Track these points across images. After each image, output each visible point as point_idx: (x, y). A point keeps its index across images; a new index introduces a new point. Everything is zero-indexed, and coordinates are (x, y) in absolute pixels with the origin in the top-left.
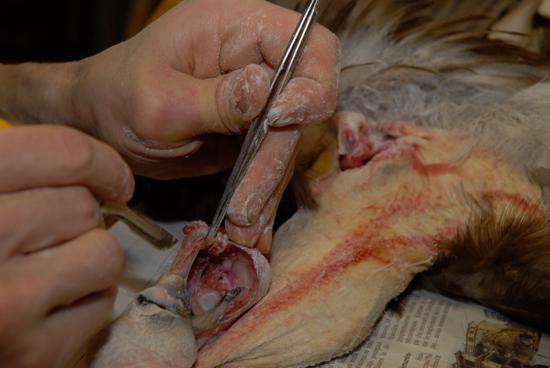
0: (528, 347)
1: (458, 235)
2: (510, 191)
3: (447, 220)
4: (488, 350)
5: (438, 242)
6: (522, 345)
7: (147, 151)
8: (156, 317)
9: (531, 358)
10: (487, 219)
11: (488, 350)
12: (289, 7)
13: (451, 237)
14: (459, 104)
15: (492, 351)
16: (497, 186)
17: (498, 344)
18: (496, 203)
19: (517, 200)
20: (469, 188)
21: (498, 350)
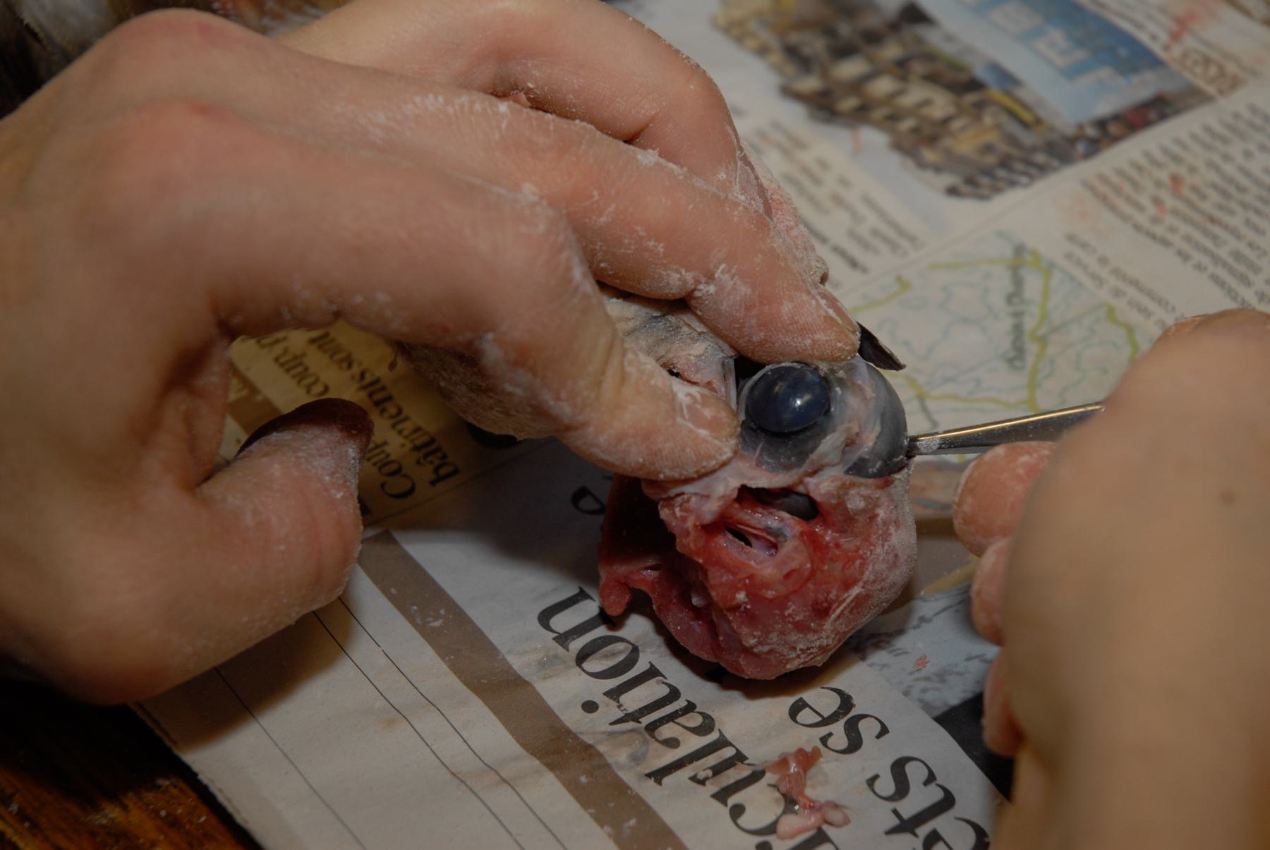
15: (816, 45)
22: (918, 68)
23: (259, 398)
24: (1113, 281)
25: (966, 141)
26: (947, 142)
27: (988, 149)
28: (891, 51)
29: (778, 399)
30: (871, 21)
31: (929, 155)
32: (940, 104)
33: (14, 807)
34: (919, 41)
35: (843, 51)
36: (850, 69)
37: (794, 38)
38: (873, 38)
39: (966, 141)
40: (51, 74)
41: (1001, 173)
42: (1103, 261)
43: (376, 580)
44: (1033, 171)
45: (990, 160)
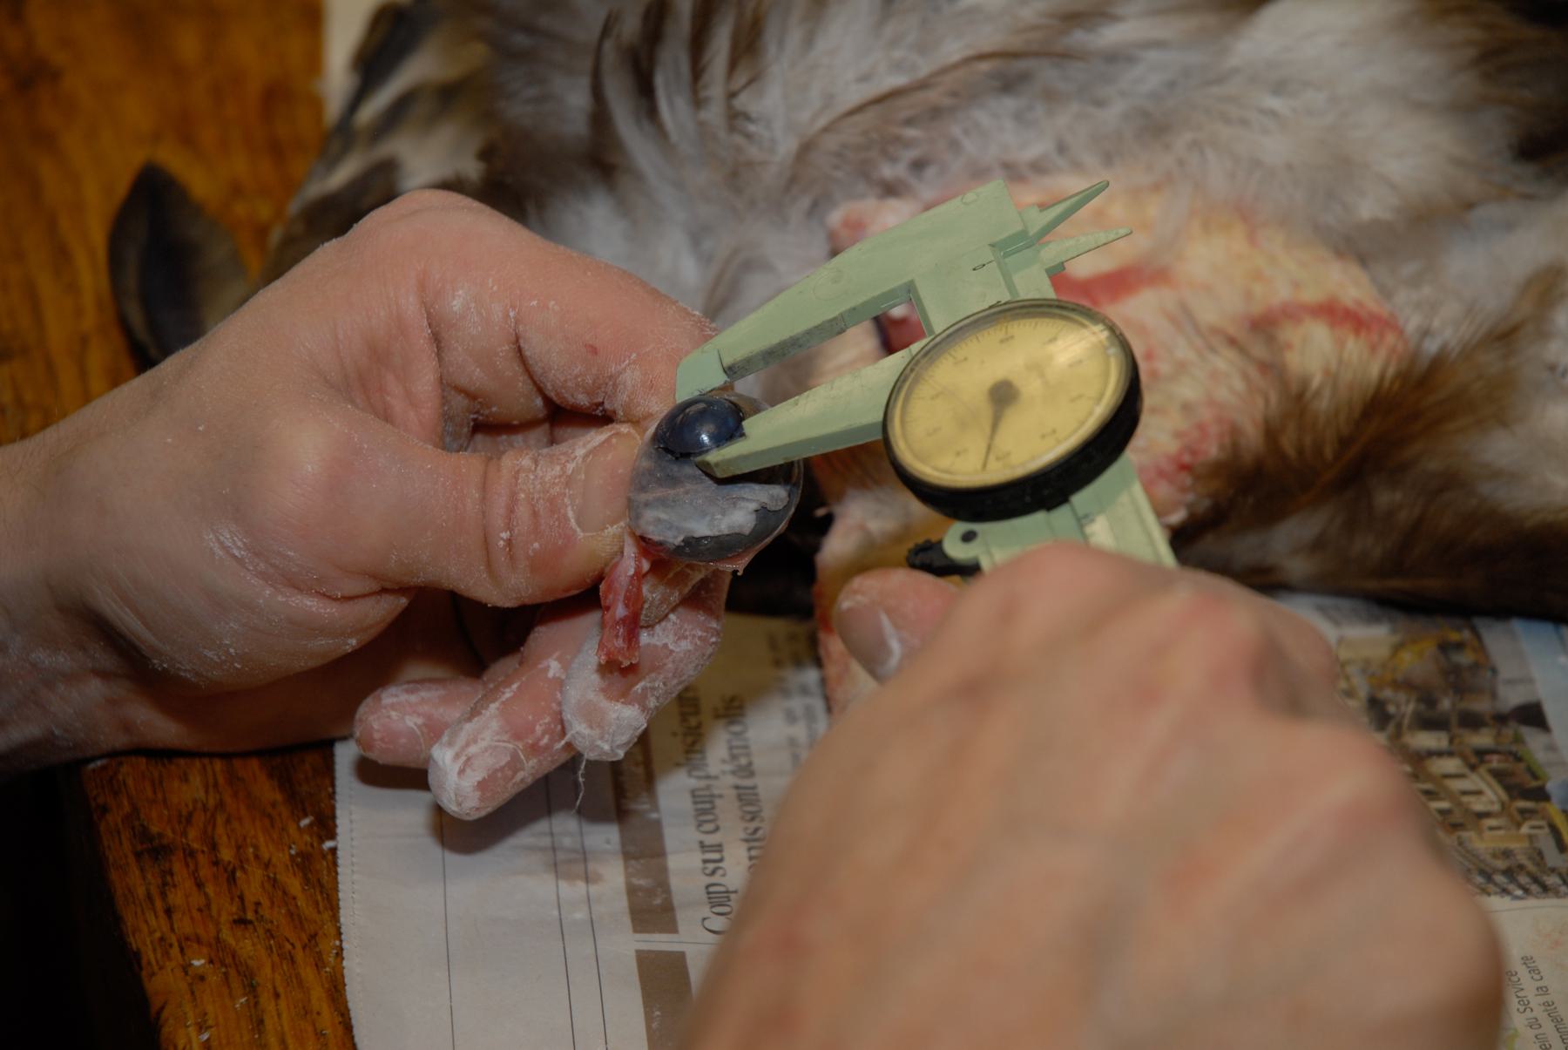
0: (1476, 667)
1: (1235, 447)
2: (1311, 295)
3: (1187, 408)
4: (1398, 706)
5: (1184, 467)
6: (1456, 670)
7: (573, 522)
8: (731, 422)
9: (1494, 695)
10: (1297, 399)
11: (1398, 706)
12: (12, 441)
13: (1212, 451)
14: (1100, 103)
15: (1407, 707)
16: (1282, 293)
17: (1407, 685)
18: (1289, 333)
19: (1333, 312)
20: (1208, 314)
21: (1419, 700)
22: (1495, 762)
23: (329, 844)
24: (1539, 1013)
25: (1484, 842)
26: (1468, 835)
27: (1507, 854)
28: (1483, 739)
29: (1469, 880)
30: (1481, 706)
31: (1448, 840)
32: (1489, 796)
33: (205, 1036)
34: (1518, 740)
35: (1429, 723)
36: (1426, 740)
37: (1387, 693)
38: (1472, 722)
39: (1484, 842)
40: (64, 415)
41: (1500, 879)
42: (1543, 990)
43: (687, 983)
44: (1534, 888)
45: (1501, 864)
